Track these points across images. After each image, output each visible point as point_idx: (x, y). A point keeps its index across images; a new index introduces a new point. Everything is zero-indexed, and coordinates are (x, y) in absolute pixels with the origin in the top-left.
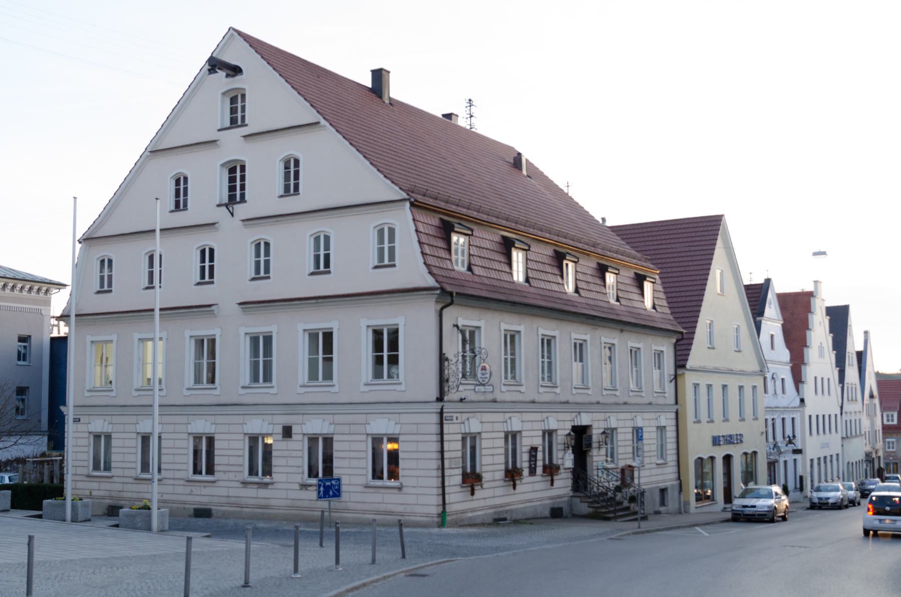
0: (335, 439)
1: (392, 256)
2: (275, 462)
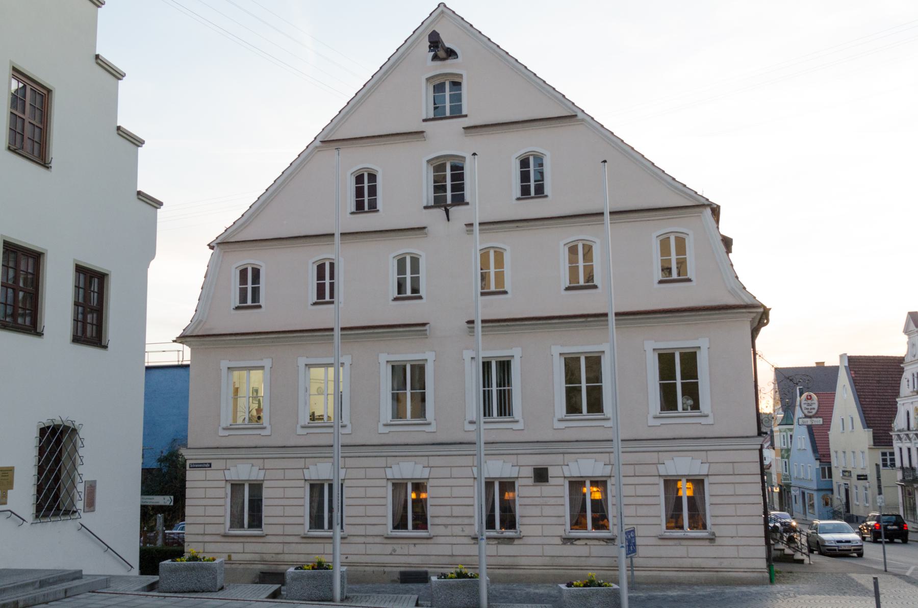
1: (256, 297)
2: (265, 511)
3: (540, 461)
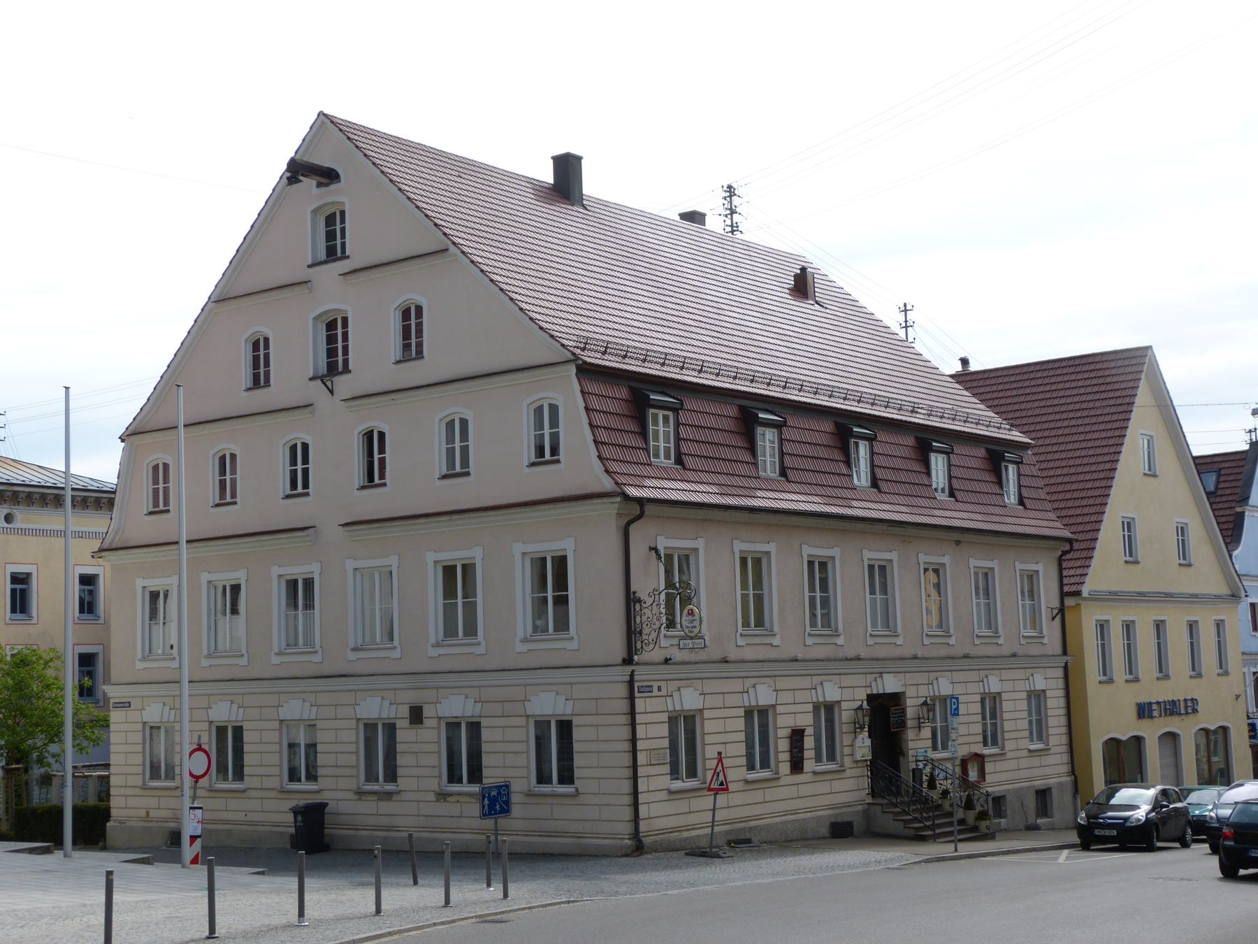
0: (574, 723)
1: (465, 462)
3: (412, 697)
